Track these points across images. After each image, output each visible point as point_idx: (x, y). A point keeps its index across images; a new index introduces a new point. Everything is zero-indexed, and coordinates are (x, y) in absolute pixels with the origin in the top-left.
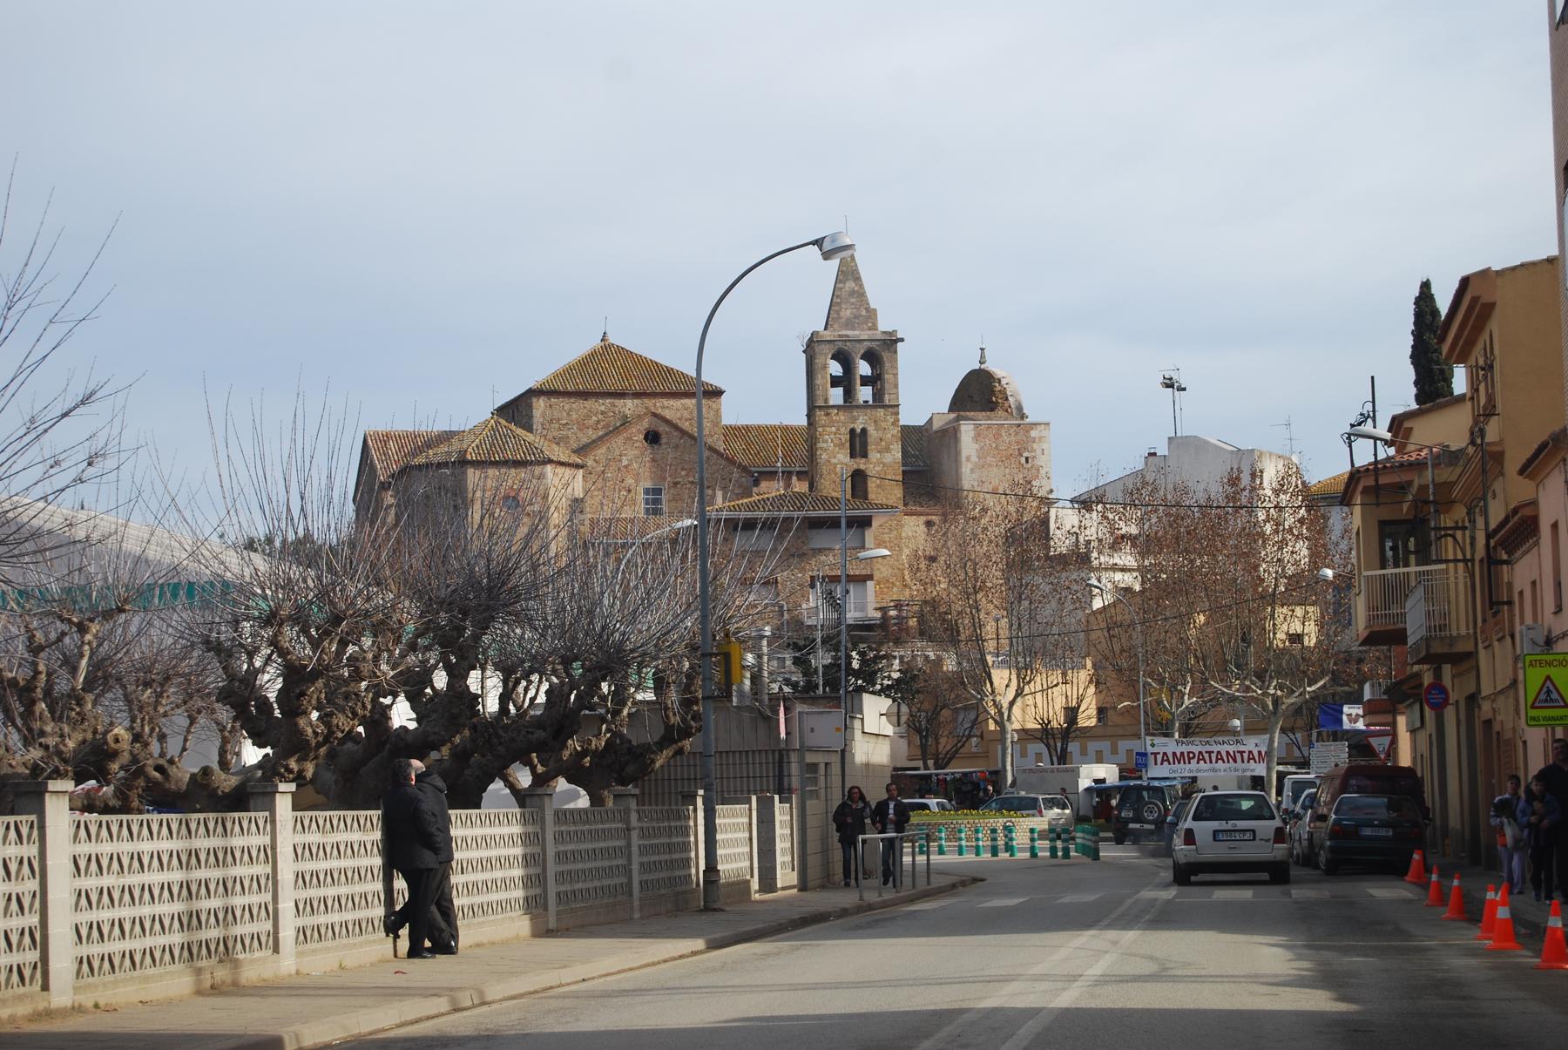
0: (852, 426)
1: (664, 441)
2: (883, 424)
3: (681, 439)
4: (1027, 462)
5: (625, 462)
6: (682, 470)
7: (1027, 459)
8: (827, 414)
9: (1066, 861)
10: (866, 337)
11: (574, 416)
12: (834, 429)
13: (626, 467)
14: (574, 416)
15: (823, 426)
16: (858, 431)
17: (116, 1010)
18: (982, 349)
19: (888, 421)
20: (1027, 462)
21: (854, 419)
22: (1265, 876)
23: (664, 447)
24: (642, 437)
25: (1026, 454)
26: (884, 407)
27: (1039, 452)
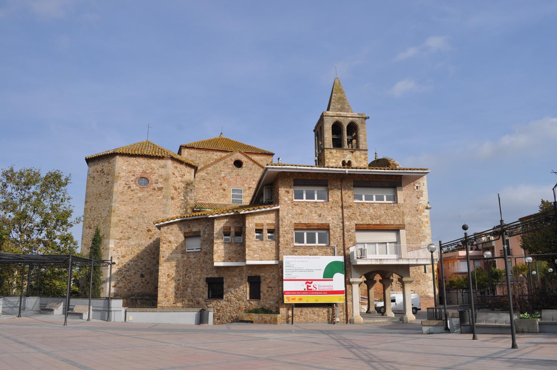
0: (343, 159)
1: (244, 165)
2: (359, 159)
3: (253, 165)
4: (417, 188)
5: (223, 175)
6: (253, 181)
7: (417, 187)
8: (331, 153)
9: (349, 326)
10: (350, 116)
11: (202, 160)
12: (334, 160)
13: (223, 177)
14: (202, 160)
15: (329, 159)
16: (347, 162)
17: (351, 206)
18: (375, 153)
19: (362, 158)
20: (417, 188)
21: (344, 156)
22: (326, 293)
23: (244, 168)
24: (233, 163)
25: (416, 185)
26: (360, 150)
27: (422, 184)
